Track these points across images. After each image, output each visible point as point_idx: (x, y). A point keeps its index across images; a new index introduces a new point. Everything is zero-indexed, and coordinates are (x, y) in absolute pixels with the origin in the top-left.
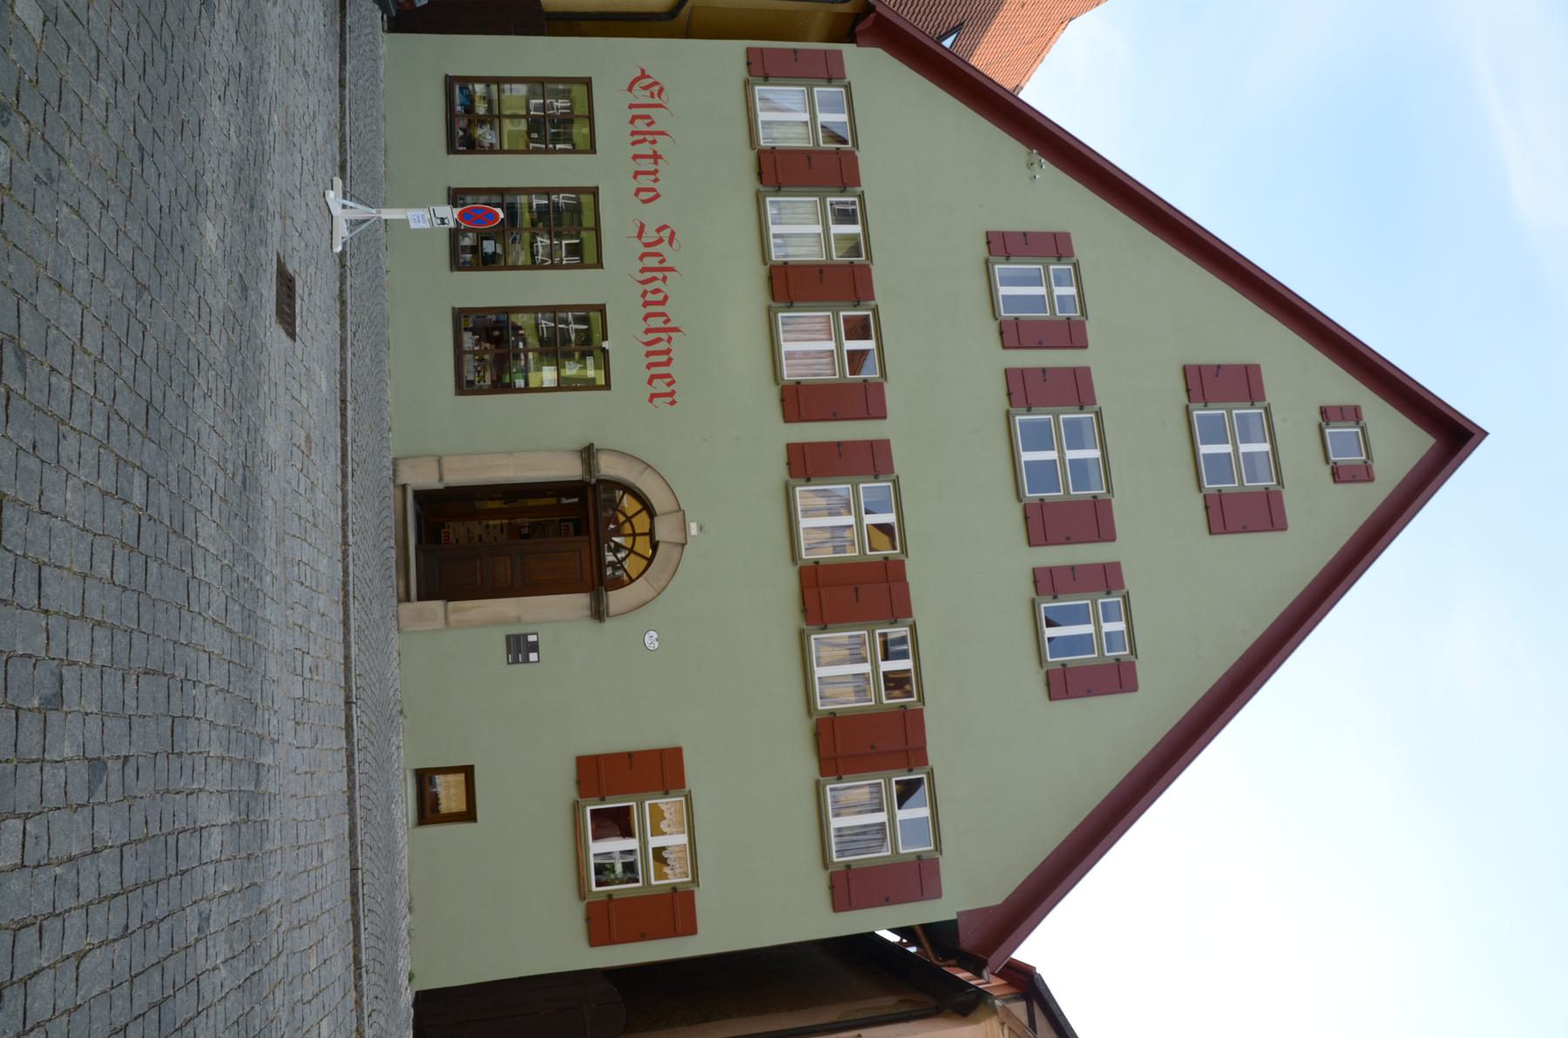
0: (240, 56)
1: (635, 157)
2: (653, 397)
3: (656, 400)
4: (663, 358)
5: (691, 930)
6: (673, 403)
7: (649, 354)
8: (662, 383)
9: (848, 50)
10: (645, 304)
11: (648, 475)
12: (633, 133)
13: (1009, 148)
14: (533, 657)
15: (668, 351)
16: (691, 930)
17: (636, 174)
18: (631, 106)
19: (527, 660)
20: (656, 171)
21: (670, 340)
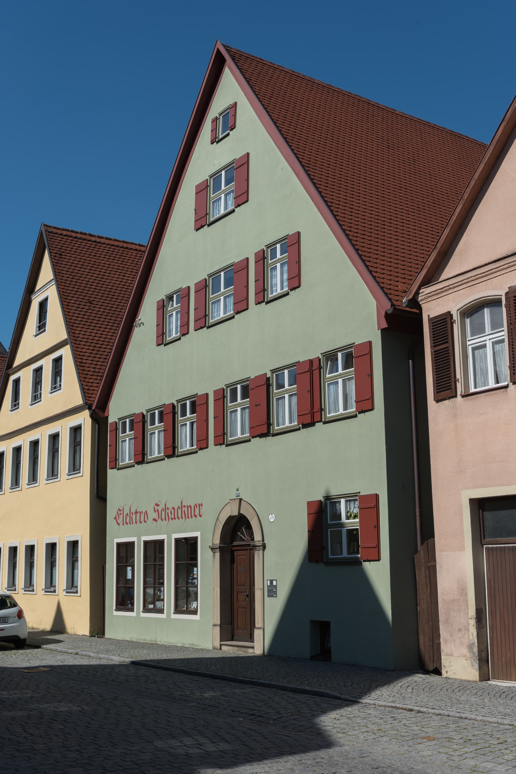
0: (399, 770)
1: (136, 523)
2: (200, 516)
3: (201, 514)
4: (189, 508)
5: (377, 496)
6: (202, 505)
7: (188, 517)
8: (190, 511)
9: (111, 420)
10: (175, 519)
11: (220, 518)
12: (130, 524)
13: (487, 262)
14: (274, 583)
15: (188, 507)
16: (377, 496)
17: (141, 522)
18: (123, 524)
19: (276, 586)
20: (140, 512)
21: (184, 506)
